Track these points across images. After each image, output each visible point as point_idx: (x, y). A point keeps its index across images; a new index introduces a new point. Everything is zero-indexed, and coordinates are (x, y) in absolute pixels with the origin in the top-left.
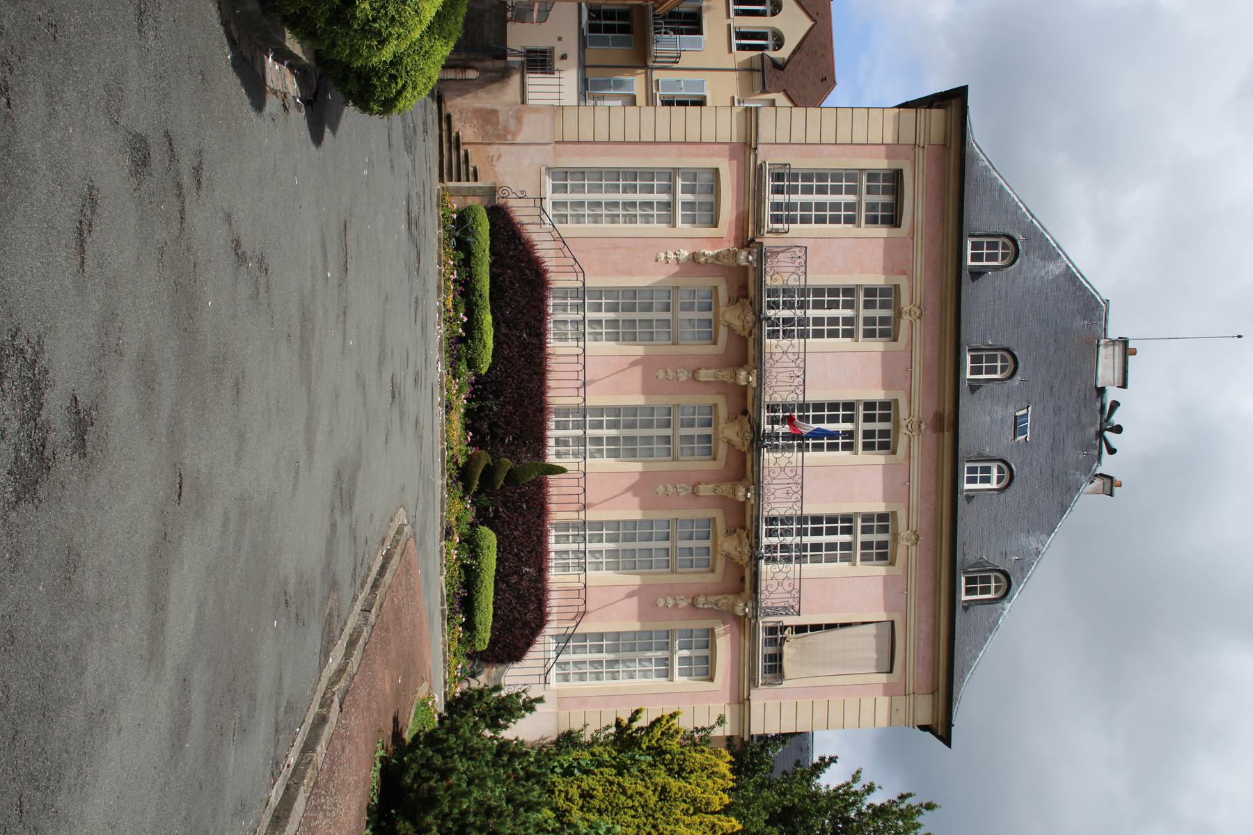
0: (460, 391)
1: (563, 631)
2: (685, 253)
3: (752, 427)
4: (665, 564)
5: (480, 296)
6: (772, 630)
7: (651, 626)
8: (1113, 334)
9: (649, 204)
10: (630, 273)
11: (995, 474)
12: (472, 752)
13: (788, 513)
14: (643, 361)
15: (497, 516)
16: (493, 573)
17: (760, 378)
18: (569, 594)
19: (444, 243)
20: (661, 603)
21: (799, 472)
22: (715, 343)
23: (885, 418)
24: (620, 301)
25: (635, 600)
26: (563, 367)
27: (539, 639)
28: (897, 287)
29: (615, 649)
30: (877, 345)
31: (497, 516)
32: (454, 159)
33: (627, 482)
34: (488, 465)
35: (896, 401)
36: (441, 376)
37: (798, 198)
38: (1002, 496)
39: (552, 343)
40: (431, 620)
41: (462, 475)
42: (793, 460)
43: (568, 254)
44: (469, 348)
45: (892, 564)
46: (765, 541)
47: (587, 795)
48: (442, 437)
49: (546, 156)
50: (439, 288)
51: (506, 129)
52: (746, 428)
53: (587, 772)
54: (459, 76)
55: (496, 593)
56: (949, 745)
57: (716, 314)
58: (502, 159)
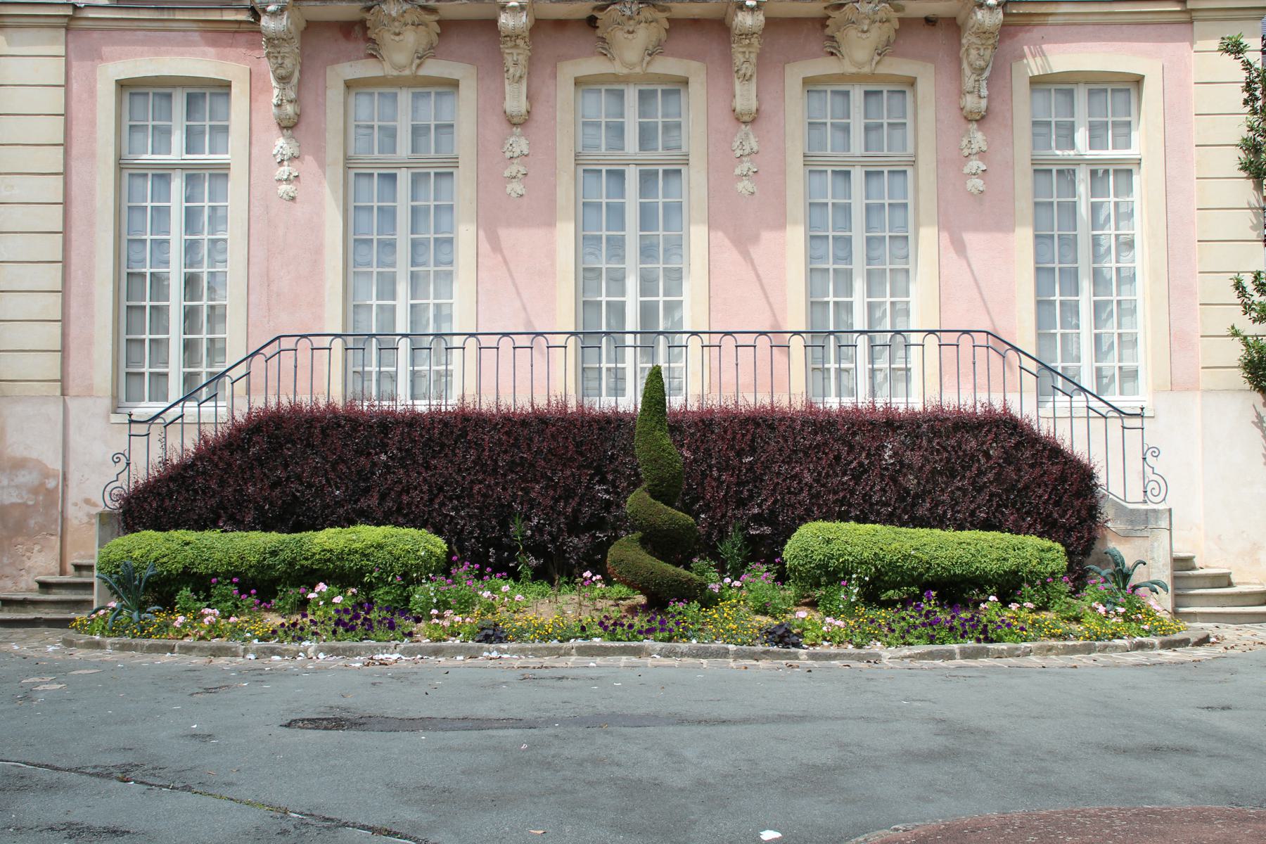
1: (1030, 381)
2: (281, 144)
4: (898, 179)
5: (274, 553)
7: (1024, 205)
9: (191, 217)
10: (318, 250)
14: (489, 224)
20: (977, 183)
24: (375, 270)
25: (970, 238)
27: (1044, 428)
29: (1071, 279)
33: (729, 255)
34: (643, 542)
43: (242, 369)
51: (35, 491)
55: (941, 523)
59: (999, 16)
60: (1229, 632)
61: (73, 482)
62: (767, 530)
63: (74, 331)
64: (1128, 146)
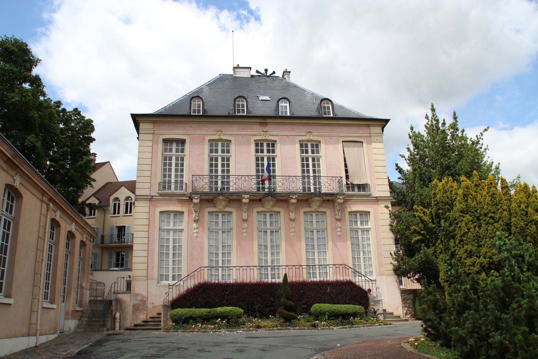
0: (251, 322)
2: (195, 225)
3: (266, 197)
4: (323, 232)
5: (209, 312)
6: (348, 188)
8: (231, 72)
11: (284, 104)
12: (476, 327)
13: (301, 182)
15: (306, 304)
16: (330, 305)
17: (246, 193)
18: (338, 272)
19: (185, 330)
20: (339, 233)
21: (284, 177)
22: (232, 212)
23: (262, 145)
26: (241, 276)
28: (209, 141)
30: (232, 148)
31: (306, 304)
32: (152, 324)
34: (284, 308)
35: (255, 141)
36: (244, 331)
37: (173, 179)
38: (292, 102)
39: (232, 281)
40: (357, 336)
41: (289, 320)
42: (279, 180)
44: (232, 318)
45: (320, 142)
46: (312, 191)
47: (470, 254)
48: (272, 330)
49: (153, 284)
50: (204, 332)
51: (141, 301)
52: (266, 197)
53: (453, 255)
54: (118, 320)
56: (389, 120)
57: (220, 212)
58: (154, 302)
59: (343, 200)
60: (395, 323)
61: (149, 299)
62: (305, 306)
63: (149, 265)
64: (368, 225)
